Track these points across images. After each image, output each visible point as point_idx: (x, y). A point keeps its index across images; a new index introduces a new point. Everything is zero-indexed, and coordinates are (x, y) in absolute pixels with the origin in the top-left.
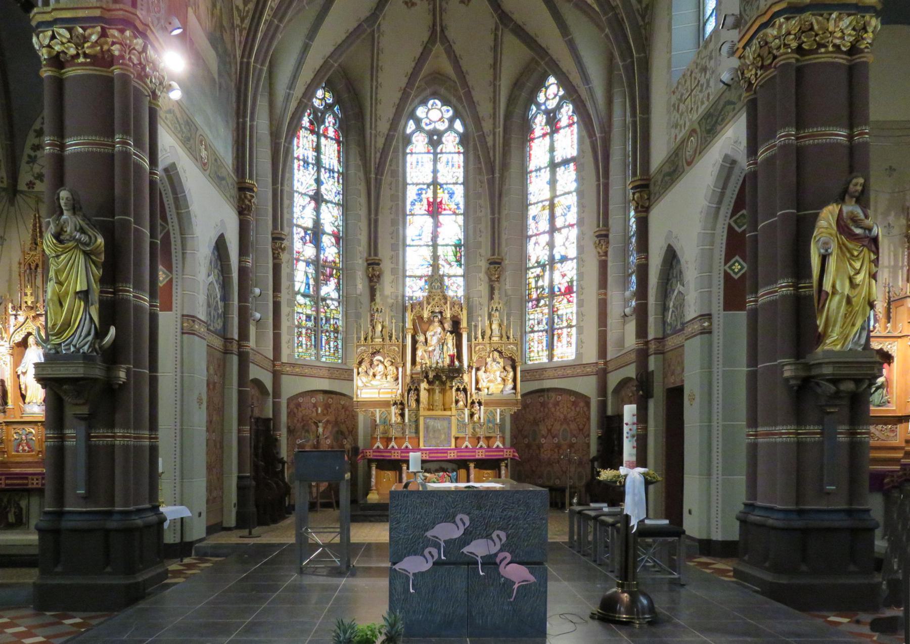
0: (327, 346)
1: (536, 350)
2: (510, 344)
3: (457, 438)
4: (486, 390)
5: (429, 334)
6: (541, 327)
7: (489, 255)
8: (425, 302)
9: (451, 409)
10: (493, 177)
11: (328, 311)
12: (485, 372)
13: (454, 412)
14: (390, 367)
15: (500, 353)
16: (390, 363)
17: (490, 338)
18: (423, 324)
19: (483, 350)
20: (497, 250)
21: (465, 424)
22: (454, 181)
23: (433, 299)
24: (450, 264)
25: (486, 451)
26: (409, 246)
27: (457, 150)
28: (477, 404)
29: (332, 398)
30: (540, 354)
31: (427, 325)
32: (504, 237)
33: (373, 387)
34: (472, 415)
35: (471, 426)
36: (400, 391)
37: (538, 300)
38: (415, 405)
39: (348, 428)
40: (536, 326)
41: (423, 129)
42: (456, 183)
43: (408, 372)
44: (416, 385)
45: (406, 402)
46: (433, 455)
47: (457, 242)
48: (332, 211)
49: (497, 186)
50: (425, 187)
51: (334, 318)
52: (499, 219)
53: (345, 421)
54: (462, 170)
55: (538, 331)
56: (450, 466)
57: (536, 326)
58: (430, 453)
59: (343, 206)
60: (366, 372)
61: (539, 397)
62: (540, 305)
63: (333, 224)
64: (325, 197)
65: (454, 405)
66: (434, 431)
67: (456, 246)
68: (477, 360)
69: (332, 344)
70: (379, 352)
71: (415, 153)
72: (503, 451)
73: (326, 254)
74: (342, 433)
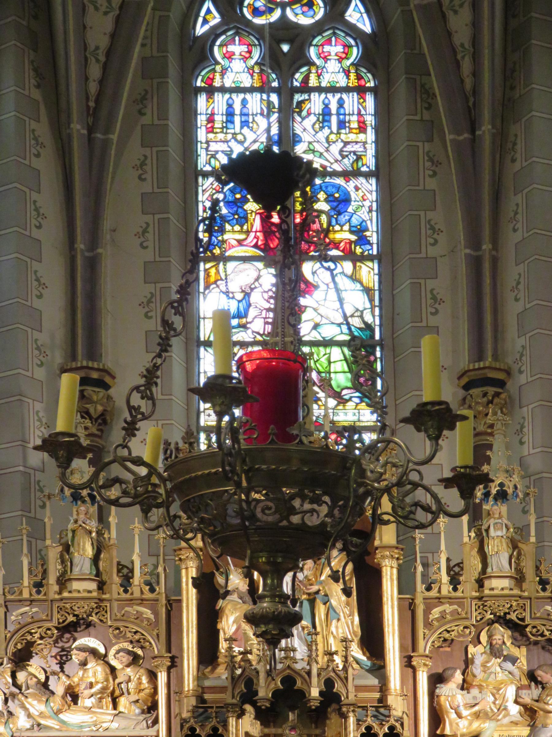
7: (464, 362)
10: (474, 141)
12: (465, 686)
14: (129, 671)
16: (127, 659)
17: (480, 583)
19: (457, 617)
24: (337, 396)
27: (353, 81)
41: (248, 23)
42: (355, 173)
44: (214, 722)
49: (486, 177)
52: (495, 261)
54: (370, 135)
60: (45, 685)
68: (436, 649)
70: (89, 625)
71: (223, 90)
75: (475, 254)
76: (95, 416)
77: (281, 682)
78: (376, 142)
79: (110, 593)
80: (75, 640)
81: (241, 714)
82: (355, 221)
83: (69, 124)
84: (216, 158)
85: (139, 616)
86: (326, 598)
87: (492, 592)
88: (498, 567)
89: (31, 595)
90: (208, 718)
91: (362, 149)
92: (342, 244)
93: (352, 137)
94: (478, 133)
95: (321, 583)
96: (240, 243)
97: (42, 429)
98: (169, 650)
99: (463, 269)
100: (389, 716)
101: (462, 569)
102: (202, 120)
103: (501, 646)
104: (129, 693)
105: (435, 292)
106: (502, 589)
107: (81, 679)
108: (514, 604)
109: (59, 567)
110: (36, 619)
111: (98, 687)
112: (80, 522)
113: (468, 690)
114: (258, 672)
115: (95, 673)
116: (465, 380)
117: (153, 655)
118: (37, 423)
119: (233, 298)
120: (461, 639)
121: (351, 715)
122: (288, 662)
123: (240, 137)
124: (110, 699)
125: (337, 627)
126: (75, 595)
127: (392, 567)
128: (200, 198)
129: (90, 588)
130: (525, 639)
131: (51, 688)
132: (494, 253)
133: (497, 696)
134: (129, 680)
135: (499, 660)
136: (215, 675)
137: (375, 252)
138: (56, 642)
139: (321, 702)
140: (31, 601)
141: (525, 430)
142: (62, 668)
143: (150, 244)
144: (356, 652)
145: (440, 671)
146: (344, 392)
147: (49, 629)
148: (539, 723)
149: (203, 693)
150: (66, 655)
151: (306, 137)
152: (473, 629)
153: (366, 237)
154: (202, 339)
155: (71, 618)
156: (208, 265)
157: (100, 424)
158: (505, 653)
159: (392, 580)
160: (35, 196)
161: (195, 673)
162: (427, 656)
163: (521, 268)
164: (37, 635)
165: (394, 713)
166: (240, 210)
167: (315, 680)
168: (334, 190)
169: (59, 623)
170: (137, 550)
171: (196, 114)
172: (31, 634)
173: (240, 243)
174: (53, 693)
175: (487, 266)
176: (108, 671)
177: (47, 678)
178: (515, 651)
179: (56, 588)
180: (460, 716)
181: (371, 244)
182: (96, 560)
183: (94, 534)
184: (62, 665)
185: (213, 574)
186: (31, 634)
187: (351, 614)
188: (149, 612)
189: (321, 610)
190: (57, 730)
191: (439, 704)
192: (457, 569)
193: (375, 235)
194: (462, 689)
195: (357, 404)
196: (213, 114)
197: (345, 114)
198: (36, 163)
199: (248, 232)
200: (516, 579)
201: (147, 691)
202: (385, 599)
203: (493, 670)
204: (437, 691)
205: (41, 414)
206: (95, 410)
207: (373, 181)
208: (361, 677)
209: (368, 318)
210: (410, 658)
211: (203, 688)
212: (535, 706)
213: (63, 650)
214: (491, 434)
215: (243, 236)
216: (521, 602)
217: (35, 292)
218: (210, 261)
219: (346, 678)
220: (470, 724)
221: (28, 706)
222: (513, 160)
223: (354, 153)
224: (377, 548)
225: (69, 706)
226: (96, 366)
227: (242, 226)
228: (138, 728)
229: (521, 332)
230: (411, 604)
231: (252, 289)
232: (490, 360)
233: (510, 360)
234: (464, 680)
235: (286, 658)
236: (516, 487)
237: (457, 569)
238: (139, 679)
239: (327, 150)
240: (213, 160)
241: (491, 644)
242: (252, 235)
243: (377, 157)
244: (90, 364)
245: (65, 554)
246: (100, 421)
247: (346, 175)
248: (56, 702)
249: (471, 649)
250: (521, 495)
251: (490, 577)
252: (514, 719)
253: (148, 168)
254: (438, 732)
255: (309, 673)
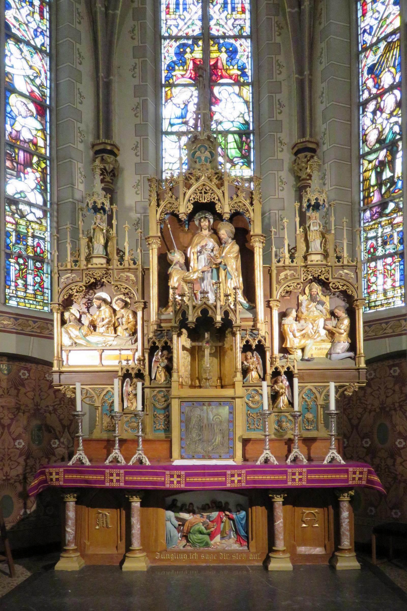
0: (20, 282)
1: (380, 288)
2: (343, 267)
3: (246, 442)
4: (299, 352)
5: (191, 252)
6: (390, 249)
8: (181, 184)
9: (233, 385)
10: (300, 13)
11: (22, 222)
13: (239, 390)
15: (324, 284)
17: (305, 258)
18: (181, 234)
19: (294, 278)
20: (308, 130)
21: (263, 415)
22: (236, 31)
23: (198, 179)
24: (231, 161)
25: (309, 472)
26: (167, 133)
28: (284, 377)
29: (26, 369)
30: (390, 294)
31: (190, 235)
32: (320, 108)
33: (89, 347)
34: (275, 397)
35: (273, 417)
36: (139, 354)
37: (383, 205)
38: (163, 379)
39: (60, 420)
40: (380, 249)
43: (153, 317)
44: (165, 339)
45: (146, 373)
46: (196, 479)
47: (242, 128)
48: (28, 57)
50: (190, 42)
51: (34, 237)
52: (311, 81)
53: (55, 410)
54: (247, 15)
55: (385, 257)
56: (232, 499)
57: (380, 249)
58: (187, 475)
59: (50, 55)
60: (80, 320)
61: (390, 367)
62: (388, 211)
63: (32, 80)
64: (14, 31)
65: (239, 376)
66: (201, 428)
67: (240, 133)
69: (30, 279)
70: (103, 285)
72: (347, 472)
73: (17, 127)
74: (49, 429)
75: (300, 77)
76: (109, 171)
77: (201, 312)
78: (251, 19)
79: (113, 265)
80: (95, 294)
81: (179, 335)
82: (240, 64)
83: (95, 4)
84: (170, 29)
85: (128, 279)
86: (225, 267)
87: (312, 263)
88: (315, 248)
89: (72, 267)
90: (162, 336)
91: (243, 23)
92: (234, 76)
93: (239, 16)
94: (302, 7)
95: (223, 257)
96: (183, 76)
97: (82, 178)
98: (143, 298)
99: (294, 86)
100: (258, 334)
101: (296, 251)
102: (163, 7)
103: (316, 295)
104: (123, 324)
105: (280, 101)
106: (317, 261)
107: (98, 316)
108: (323, 269)
109: (87, 251)
110: (74, 281)
111: (106, 321)
112: (97, 224)
113: (299, 321)
114: (188, 307)
115: (105, 312)
116: (296, 149)
117: (135, 301)
118: (79, 175)
119: (179, 107)
120: (296, 291)
121: (238, 332)
122: (204, 300)
123: (182, 17)
124: (113, 328)
125: (231, 284)
126: (94, 266)
127: (260, 248)
128: (163, 51)
129: (102, 263)
130: (328, 291)
131: (83, 322)
132: (310, 77)
133: (314, 325)
134: (123, 317)
135: (315, 304)
136: (167, 313)
137: (250, 81)
138: (85, 295)
139: (222, 324)
140: (72, 270)
141: (326, 177)
142: (88, 310)
143: (137, 75)
144: (241, 298)
145: (284, 311)
146: (235, 159)
147: (81, 287)
148: (336, 340)
149: (161, 323)
150: (91, 303)
151: (215, 16)
152: (302, 285)
153: (245, 72)
154: (164, 131)
155: (93, 280)
156: (167, 89)
157: (111, 176)
158: (318, 300)
159: (260, 255)
160: (78, 46)
161: (157, 311)
162: (278, 301)
163: (324, 85)
164: (75, 291)
165: (260, 332)
166: (183, 58)
167: (219, 311)
168: (229, 46)
169: (86, 283)
170: (127, 240)
171: (160, 4)
172: (72, 290)
173: (183, 76)
174: (83, 325)
175: (307, 83)
176: (112, 311)
177: (81, 316)
178: (323, 298)
179: (85, 263)
180: (295, 336)
181: (248, 77)
182: (106, 246)
183: (104, 231)
184: (88, 308)
185: (166, 254)
186: (72, 290)
187: (238, 276)
188: (133, 276)
189: (222, 273)
190: (85, 346)
191: (284, 329)
192: (293, 251)
193: (250, 71)
194: (296, 320)
195: (241, 166)
196: (169, 4)
197: (235, 4)
198: (79, 27)
199: (186, 70)
200: (324, 255)
201: (132, 323)
202: (256, 266)
203: (311, 309)
204: (283, 322)
205: (82, 170)
206: (109, 167)
207: (249, 41)
208: (243, 313)
209: (247, 118)
210: (269, 302)
211: (161, 320)
212: (334, 330)
213: (89, 300)
214: (310, 179)
215: (183, 73)
216: (327, 268)
217: (78, 100)
218: (168, 87)
219: (236, 311)
220: (300, 341)
221: (70, 332)
222: (320, 23)
223: (240, 25)
224: (252, 236)
225: (92, 332)
226: (109, 142)
227: (183, 67)
228: (127, 344)
229: (324, 120)
230: (269, 270)
231: (189, 102)
232: (308, 137)
233: (318, 138)
234: (297, 316)
235: (203, 298)
236: (324, 201)
237: (293, 251)
238: (128, 316)
239: (226, 23)
240: (169, 30)
241: (311, 295)
242: (189, 72)
243: (251, 27)
244: (106, 141)
245: (90, 243)
246: (111, 174)
247: (236, 37)
248: (85, 330)
249: (301, 298)
250: (327, 206)
251: (311, 254)
252: (323, 338)
253: (136, 32)
254: (283, 346)
255: (215, 307)
